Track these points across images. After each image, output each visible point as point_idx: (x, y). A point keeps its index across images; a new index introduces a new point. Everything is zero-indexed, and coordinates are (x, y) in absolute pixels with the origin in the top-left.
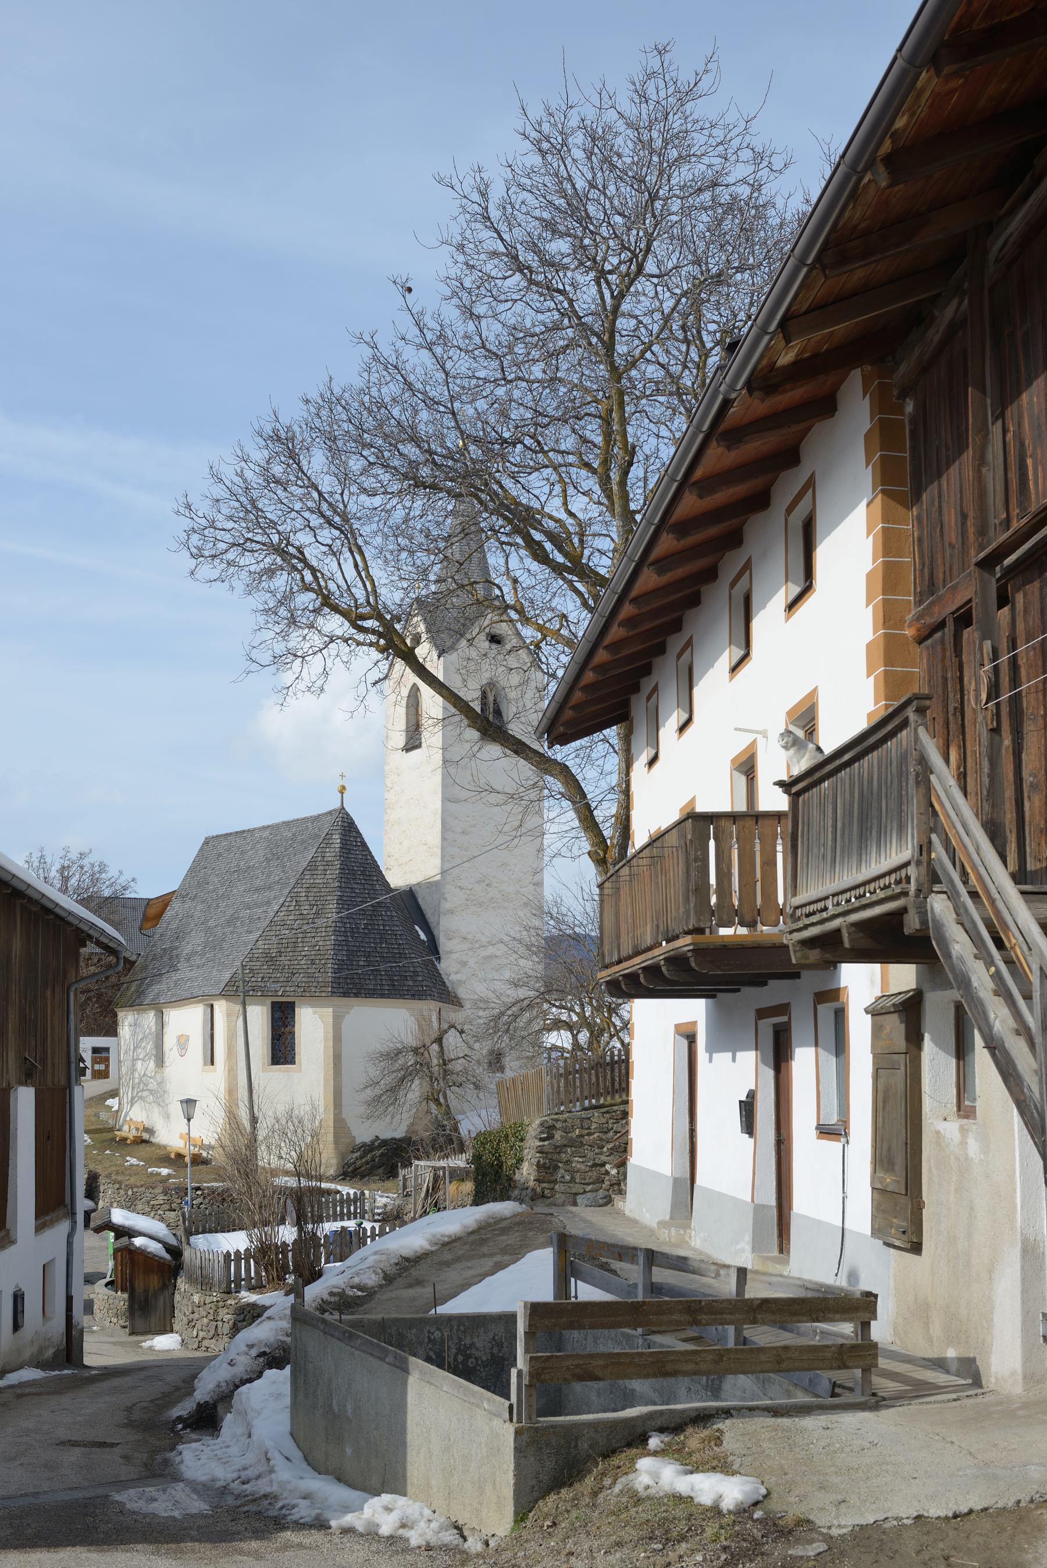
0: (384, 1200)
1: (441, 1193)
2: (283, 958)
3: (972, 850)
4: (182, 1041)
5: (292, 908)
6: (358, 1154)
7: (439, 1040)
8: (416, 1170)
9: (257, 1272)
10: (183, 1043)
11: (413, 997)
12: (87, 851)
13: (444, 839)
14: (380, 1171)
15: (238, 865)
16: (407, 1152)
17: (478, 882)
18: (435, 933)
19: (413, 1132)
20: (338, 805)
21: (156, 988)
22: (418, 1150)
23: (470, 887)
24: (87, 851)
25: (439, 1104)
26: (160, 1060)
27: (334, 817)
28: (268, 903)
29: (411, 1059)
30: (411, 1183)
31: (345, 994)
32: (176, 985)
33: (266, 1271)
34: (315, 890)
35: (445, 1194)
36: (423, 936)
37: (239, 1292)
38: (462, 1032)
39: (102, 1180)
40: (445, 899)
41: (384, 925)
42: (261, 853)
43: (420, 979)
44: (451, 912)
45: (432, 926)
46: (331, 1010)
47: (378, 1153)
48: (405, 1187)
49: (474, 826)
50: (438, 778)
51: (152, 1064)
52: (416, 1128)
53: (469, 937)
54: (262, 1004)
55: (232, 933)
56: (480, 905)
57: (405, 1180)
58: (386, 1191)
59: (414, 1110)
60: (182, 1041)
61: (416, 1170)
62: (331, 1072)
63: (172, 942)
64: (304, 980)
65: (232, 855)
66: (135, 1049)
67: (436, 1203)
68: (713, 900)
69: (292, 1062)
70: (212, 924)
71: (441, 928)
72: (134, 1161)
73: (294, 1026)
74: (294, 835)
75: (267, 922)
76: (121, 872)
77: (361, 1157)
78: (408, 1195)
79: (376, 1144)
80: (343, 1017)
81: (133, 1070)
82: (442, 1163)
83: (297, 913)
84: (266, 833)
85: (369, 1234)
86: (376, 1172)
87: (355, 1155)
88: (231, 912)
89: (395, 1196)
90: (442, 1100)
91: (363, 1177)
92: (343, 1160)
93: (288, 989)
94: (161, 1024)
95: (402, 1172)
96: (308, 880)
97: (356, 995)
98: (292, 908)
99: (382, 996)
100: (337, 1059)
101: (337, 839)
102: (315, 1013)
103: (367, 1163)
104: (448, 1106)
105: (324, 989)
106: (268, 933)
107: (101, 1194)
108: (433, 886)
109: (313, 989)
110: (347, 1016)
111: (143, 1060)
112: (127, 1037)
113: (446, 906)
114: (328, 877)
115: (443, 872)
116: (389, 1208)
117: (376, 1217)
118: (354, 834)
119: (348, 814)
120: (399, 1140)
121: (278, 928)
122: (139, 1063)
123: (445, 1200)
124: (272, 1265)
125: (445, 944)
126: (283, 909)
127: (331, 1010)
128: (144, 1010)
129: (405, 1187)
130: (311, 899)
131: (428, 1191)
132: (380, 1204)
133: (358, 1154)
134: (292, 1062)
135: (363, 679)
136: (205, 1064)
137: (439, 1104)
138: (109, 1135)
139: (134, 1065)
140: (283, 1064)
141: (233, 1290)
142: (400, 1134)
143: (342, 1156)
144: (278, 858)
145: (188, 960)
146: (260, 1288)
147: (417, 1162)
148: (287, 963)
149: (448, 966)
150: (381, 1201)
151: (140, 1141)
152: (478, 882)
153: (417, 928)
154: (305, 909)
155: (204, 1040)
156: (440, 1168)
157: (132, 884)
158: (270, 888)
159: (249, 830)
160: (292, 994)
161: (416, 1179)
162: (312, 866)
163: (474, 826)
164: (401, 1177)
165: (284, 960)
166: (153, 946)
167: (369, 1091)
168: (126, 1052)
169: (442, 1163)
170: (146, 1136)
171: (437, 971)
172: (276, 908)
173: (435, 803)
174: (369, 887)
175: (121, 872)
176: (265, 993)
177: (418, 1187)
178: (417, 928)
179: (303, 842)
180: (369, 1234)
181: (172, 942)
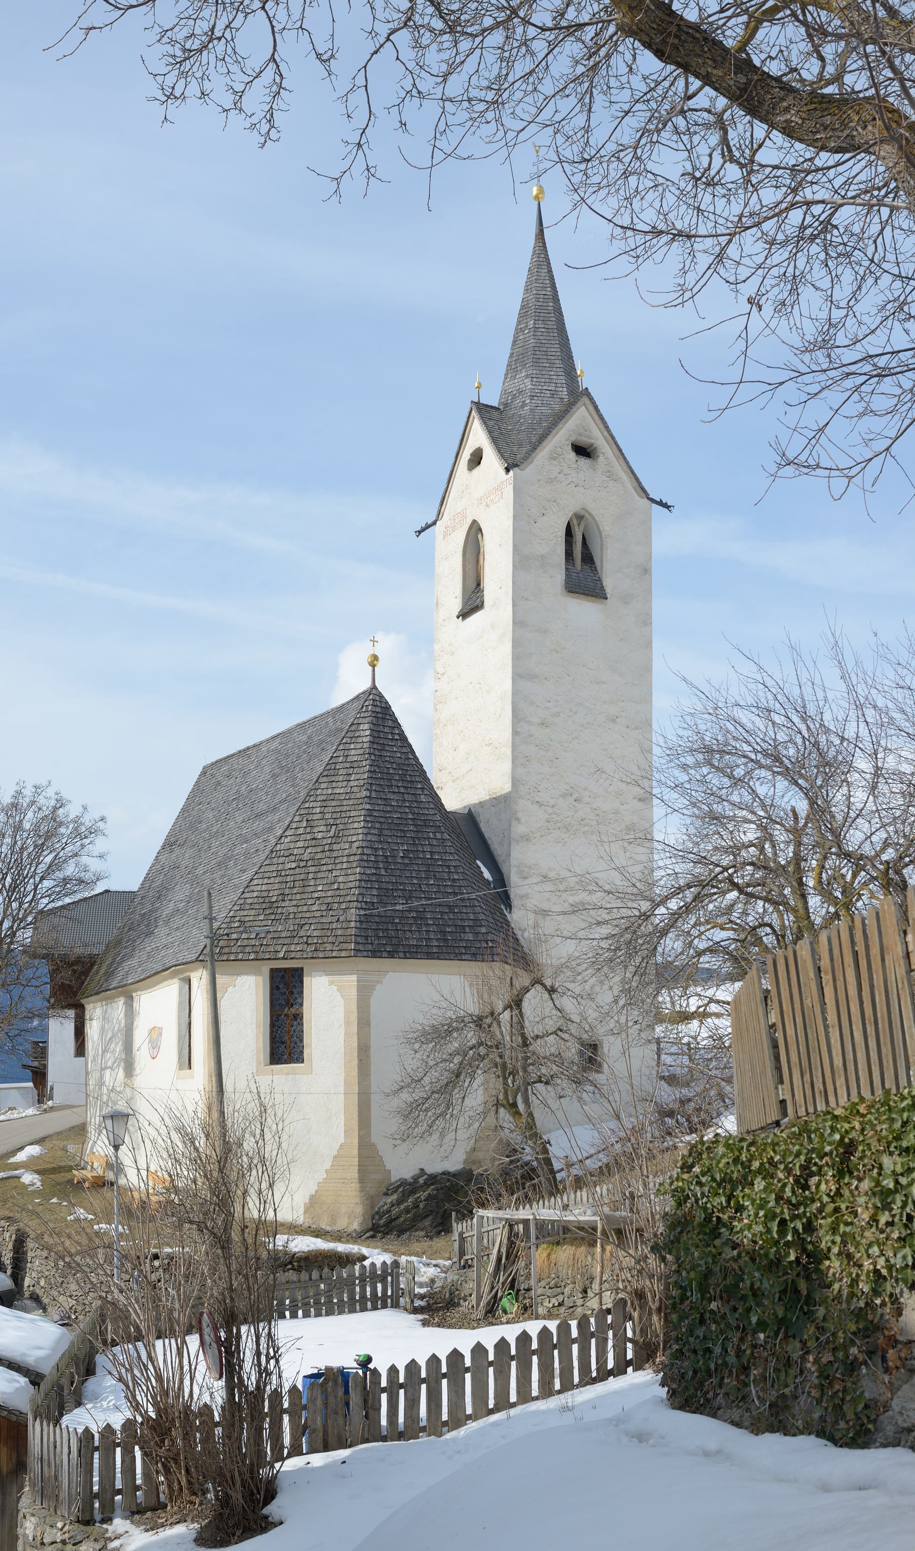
0: (431, 1272)
1: (521, 1264)
2: (287, 903)
3: (875, 951)
4: (154, 1035)
5: (301, 831)
6: (395, 1197)
7: (516, 1004)
8: (481, 1225)
9: (146, 1475)
10: (155, 1035)
11: (474, 957)
12: (45, 783)
13: (515, 733)
14: (427, 1222)
15: (238, 792)
16: (466, 1193)
17: (564, 796)
18: (504, 870)
19: (474, 1162)
20: (366, 685)
21: (126, 965)
22: (482, 1190)
23: (552, 802)
24: (45, 783)
25: (517, 1114)
26: (130, 1070)
27: (361, 702)
28: (271, 829)
29: (471, 1036)
30: (472, 1247)
31: (375, 954)
32: (149, 957)
33: (167, 1471)
34: (334, 803)
35: (527, 1266)
36: (487, 875)
37: (108, 1520)
38: (551, 991)
39: (30, 1244)
40: (518, 820)
41: (432, 853)
42: (267, 769)
43: (483, 930)
44: (526, 838)
45: (500, 860)
46: (354, 978)
47: (423, 1195)
48: (462, 1253)
49: (557, 715)
50: (507, 648)
51: (121, 1074)
52: (480, 1155)
53: (552, 875)
54: (257, 973)
55: (222, 876)
56: (567, 828)
57: (462, 1240)
58: (434, 1255)
59: (476, 1125)
60: (154, 1035)
61: (481, 1225)
62: (355, 1073)
63: (153, 904)
64: (316, 933)
65: (232, 781)
66: (103, 1052)
67: (514, 1280)
68: (97, 1505)
69: (300, 1059)
70: (200, 871)
71: (513, 862)
72: (81, 1213)
73: (301, 1005)
74: (309, 737)
75: (267, 852)
76: (85, 808)
77: (399, 1203)
78: (467, 1266)
79: (421, 1181)
80: (373, 988)
81: (101, 1083)
82: (524, 1213)
83: (309, 837)
84: (275, 745)
85: (384, 1384)
86: (421, 1225)
87: (389, 1200)
88: (224, 850)
89: (448, 1263)
90: (521, 1106)
91: (401, 1232)
92: (372, 1207)
93: (293, 948)
94: (130, 1014)
95: (458, 1228)
96: (324, 790)
97: (392, 955)
98: (301, 831)
99: (430, 956)
100: (364, 1052)
101: (365, 730)
102: (331, 983)
103: (407, 1211)
104: (531, 1115)
105: (344, 946)
106: (267, 869)
107: (29, 1265)
108: (501, 802)
109: (329, 947)
110: (378, 987)
111: (111, 1068)
112: (96, 1037)
113: (519, 829)
114: (352, 784)
115: (515, 782)
116: (438, 1284)
117: (418, 1303)
118: (390, 723)
119: (381, 696)
120: (455, 1175)
121: (281, 860)
122: (108, 1072)
123: (528, 1277)
124: (176, 1461)
125: (517, 886)
126: (289, 833)
127: (354, 978)
128: (112, 998)
129: (462, 1253)
130: (328, 816)
131: (499, 1259)
132: (424, 1279)
133: (395, 1197)
134: (300, 1059)
135: (360, 81)
136: (181, 1068)
137: (517, 1114)
138: (68, 1176)
139: (102, 1077)
140: (286, 1062)
141: (98, 1516)
142: (454, 1164)
143: (370, 1200)
144: (287, 771)
145: (167, 922)
146: (154, 1509)
147: (481, 1212)
148: (292, 910)
149: (519, 917)
150: (426, 1273)
151: (100, 1184)
152: (564, 796)
153: (478, 862)
154: (320, 830)
155: (180, 1031)
156: (518, 1222)
157: (100, 824)
158: (275, 809)
159: (255, 746)
160: (299, 955)
161: (480, 1239)
162: (330, 771)
163: (557, 715)
164: (456, 1236)
165: (288, 906)
166: (132, 913)
167: (405, 1096)
168: (94, 1060)
169: (524, 1213)
170: (110, 1176)
171: (508, 923)
172: (280, 832)
173: (504, 683)
174: (410, 798)
175: (85, 808)
176: (261, 956)
177: (483, 1252)
178: (478, 862)
179: (321, 742)
180: (384, 1384)
181: (153, 904)
